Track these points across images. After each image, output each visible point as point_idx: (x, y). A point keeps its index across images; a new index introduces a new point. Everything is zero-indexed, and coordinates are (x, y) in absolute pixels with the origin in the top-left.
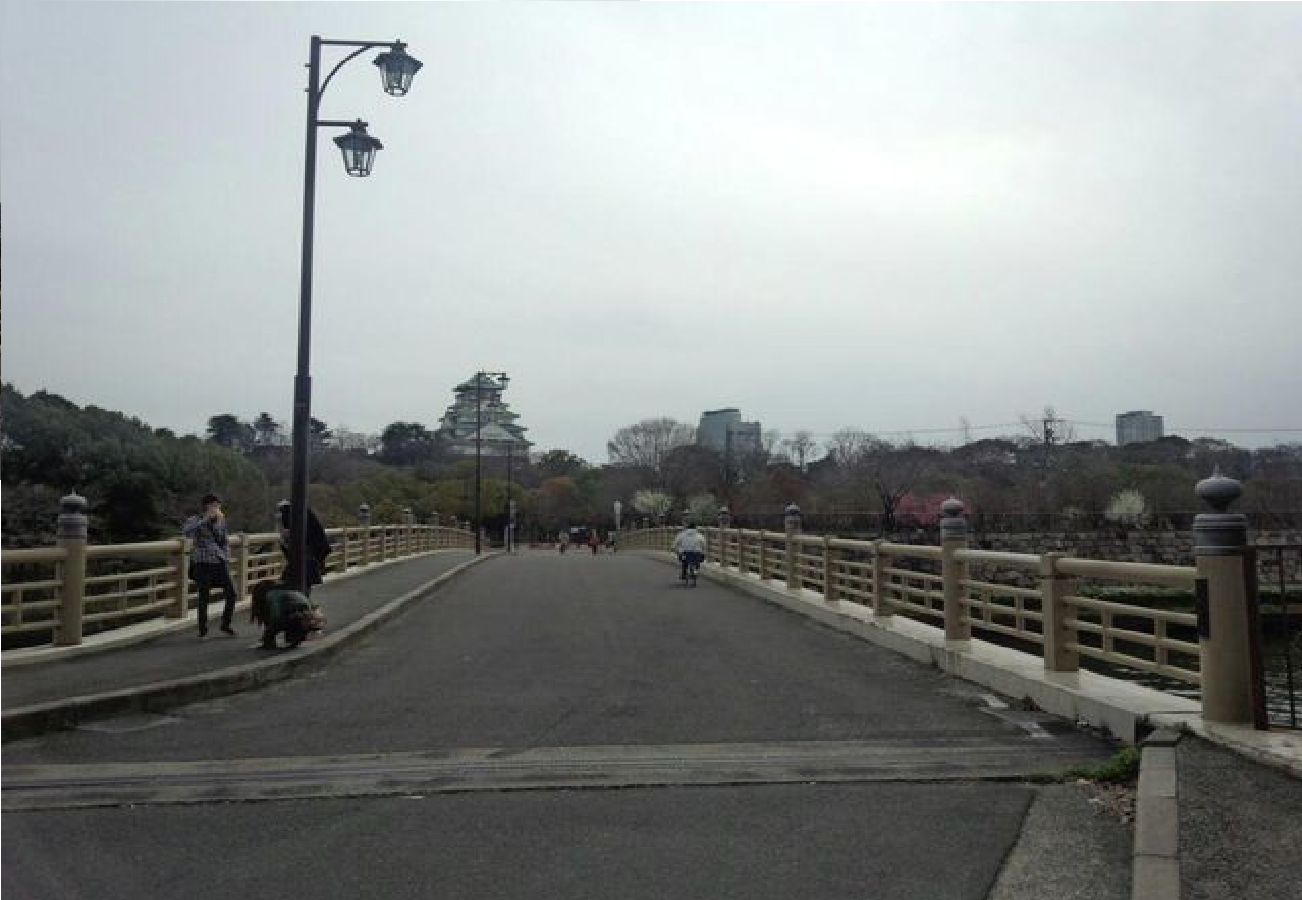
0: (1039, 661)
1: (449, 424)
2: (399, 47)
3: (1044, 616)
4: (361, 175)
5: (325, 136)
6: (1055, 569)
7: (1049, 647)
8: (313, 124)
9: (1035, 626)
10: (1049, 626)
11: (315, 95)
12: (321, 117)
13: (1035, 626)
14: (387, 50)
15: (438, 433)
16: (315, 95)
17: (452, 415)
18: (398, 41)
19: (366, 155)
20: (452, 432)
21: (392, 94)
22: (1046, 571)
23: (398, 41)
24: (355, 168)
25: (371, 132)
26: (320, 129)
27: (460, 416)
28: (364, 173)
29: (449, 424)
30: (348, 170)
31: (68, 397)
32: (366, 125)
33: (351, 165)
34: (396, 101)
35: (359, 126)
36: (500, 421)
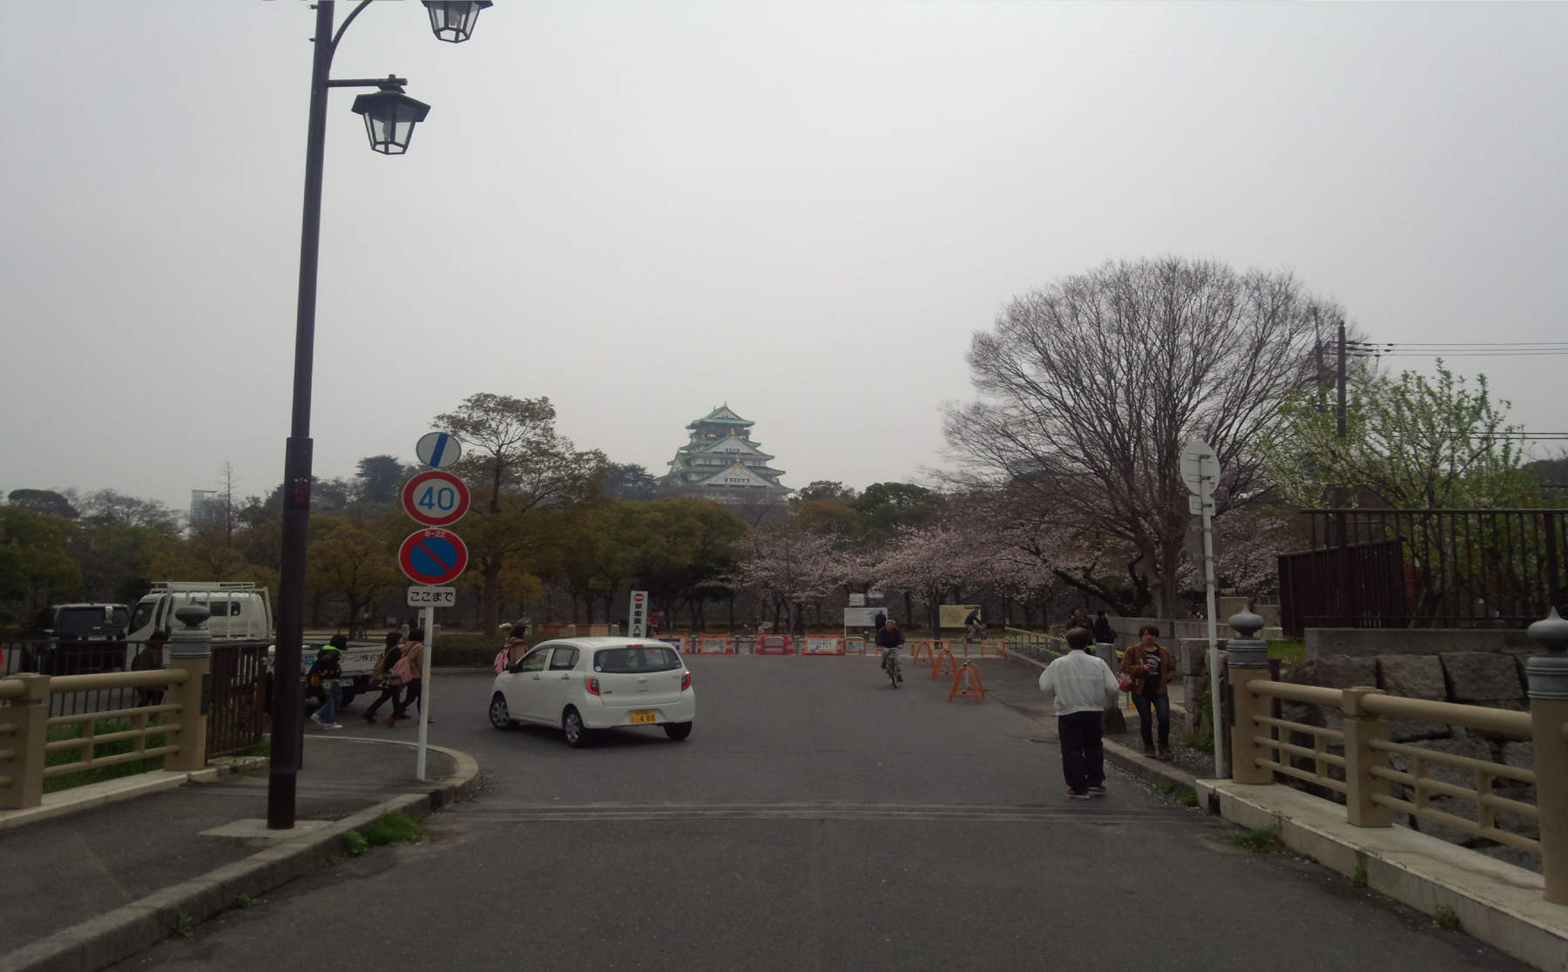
0: (1341, 811)
1: (680, 466)
2: (393, 85)
3: (1348, 761)
4: (457, 41)
5: (340, 102)
6: (1359, 706)
7: (1353, 798)
8: (321, 84)
9: (1339, 773)
10: (1352, 773)
11: (325, 46)
12: (334, 75)
13: (1339, 773)
14: (375, 90)
15: (666, 480)
16: (325, 46)
17: (686, 458)
18: (392, 76)
19: (464, 17)
20: (684, 476)
21: (386, 152)
22: (1350, 708)
23: (392, 76)
24: (446, 27)
25: (410, 92)
26: (331, 90)
27: (695, 458)
28: (462, 36)
29: (680, 466)
30: (437, 32)
31: (31, 487)
32: (404, 82)
33: (441, 24)
34: (447, 51)
35: (393, 85)
36: (750, 464)
